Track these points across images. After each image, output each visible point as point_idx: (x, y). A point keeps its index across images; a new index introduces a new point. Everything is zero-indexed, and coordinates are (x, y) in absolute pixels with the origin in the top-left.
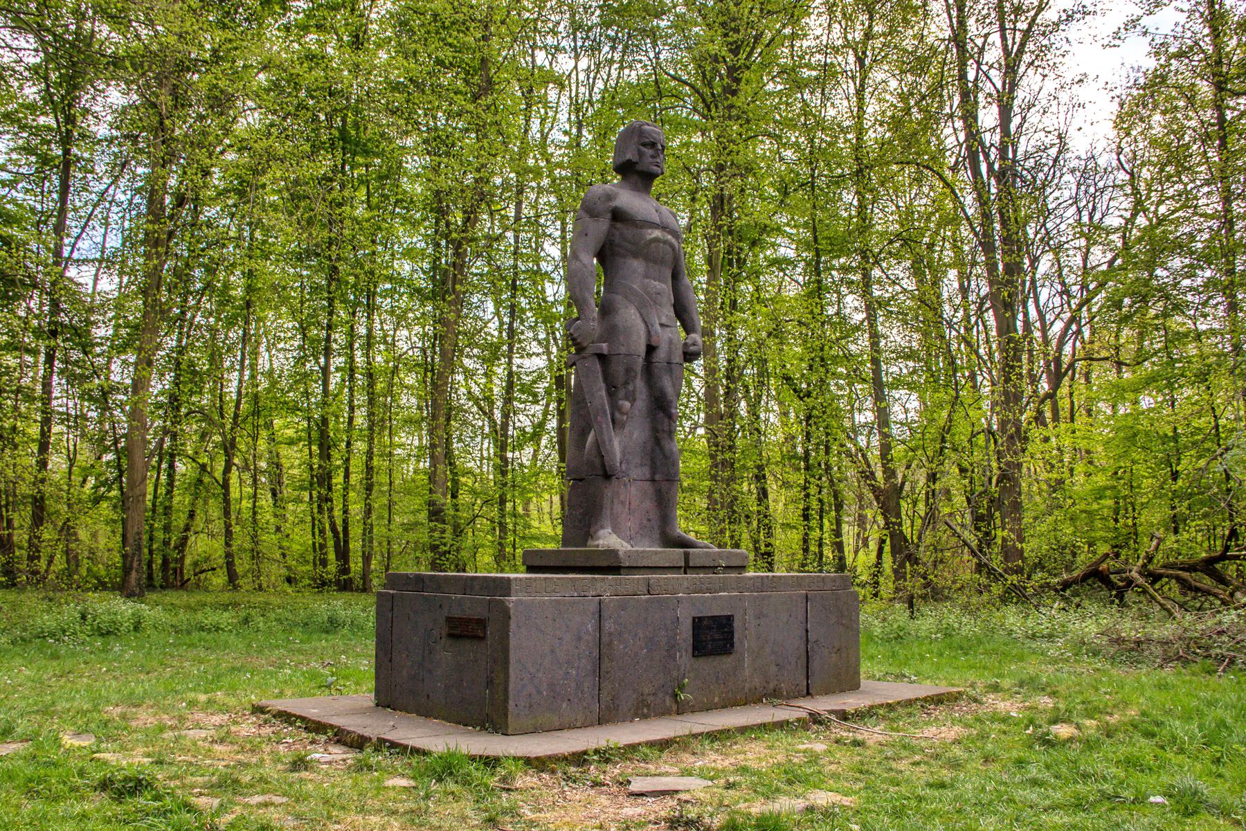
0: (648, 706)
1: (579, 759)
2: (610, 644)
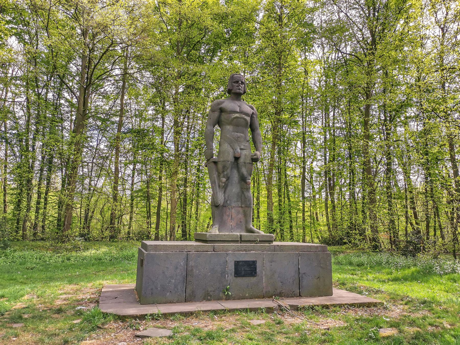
0: (211, 296)
1: (166, 316)
2: (192, 270)
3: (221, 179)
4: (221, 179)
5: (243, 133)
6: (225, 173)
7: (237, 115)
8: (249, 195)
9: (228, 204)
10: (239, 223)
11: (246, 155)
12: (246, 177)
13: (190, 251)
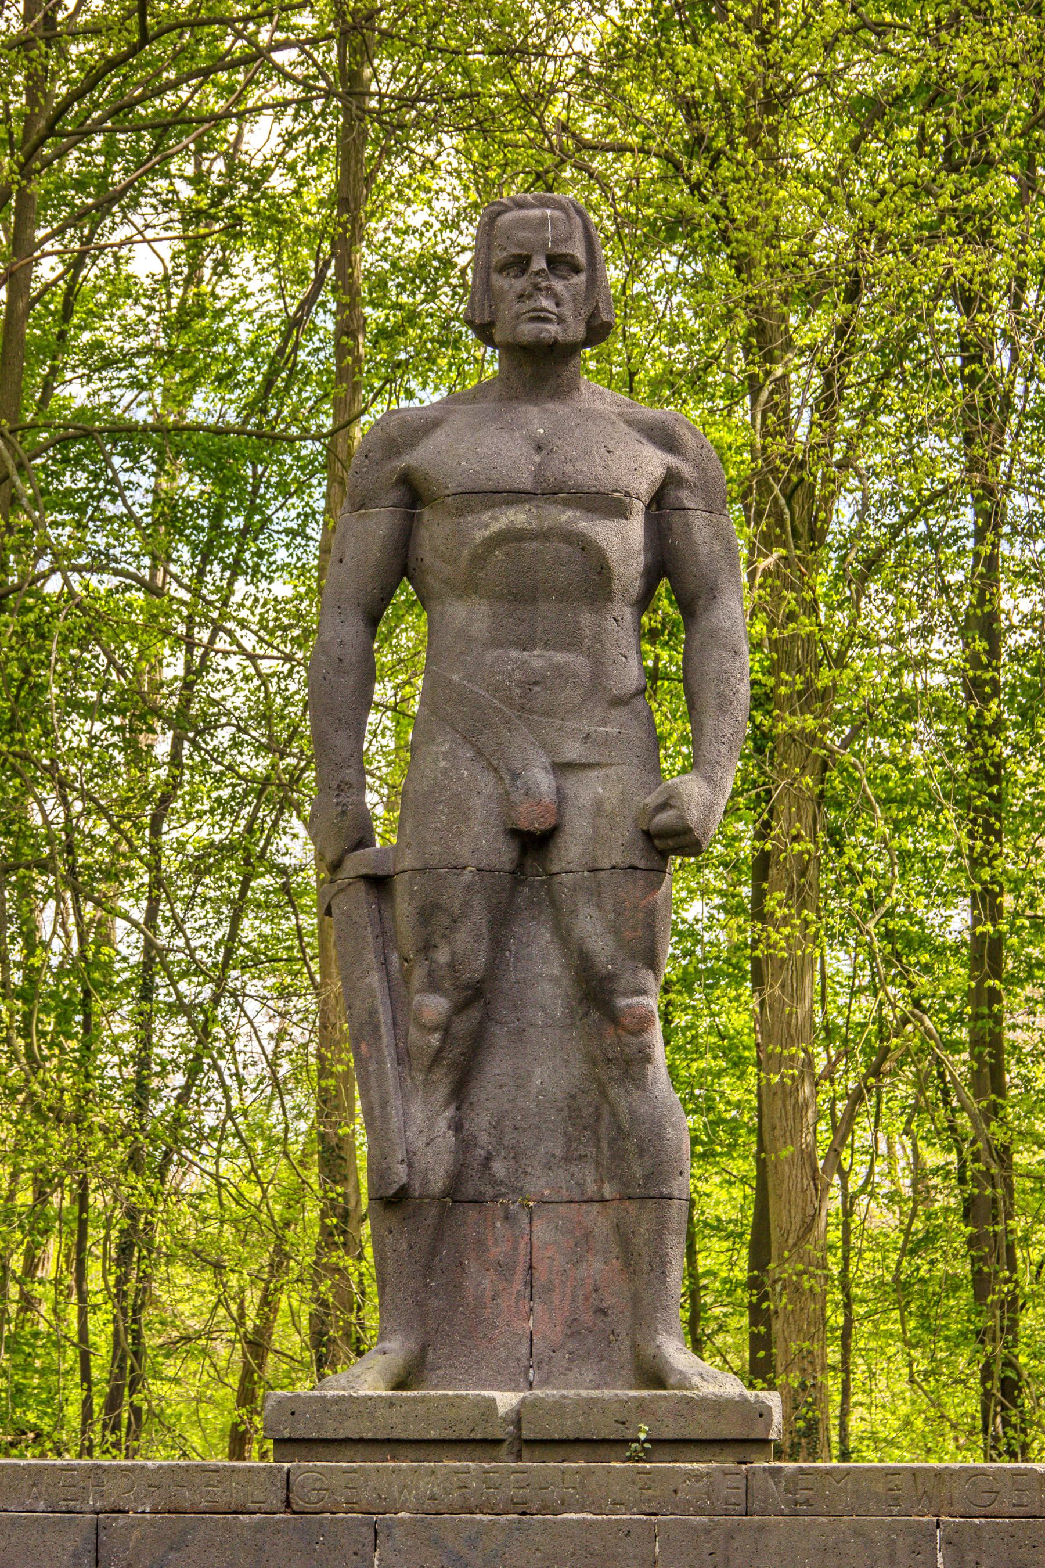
3: (417, 998)
4: (417, 998)
5: (572, 642)
6: (442, 956)
7: (516, 517)
8: (644, 1109)
9: (495, 1183)
10: (587, 1317)
11: (598, 809)
12: (612, 977)
13: (121, 1505)
